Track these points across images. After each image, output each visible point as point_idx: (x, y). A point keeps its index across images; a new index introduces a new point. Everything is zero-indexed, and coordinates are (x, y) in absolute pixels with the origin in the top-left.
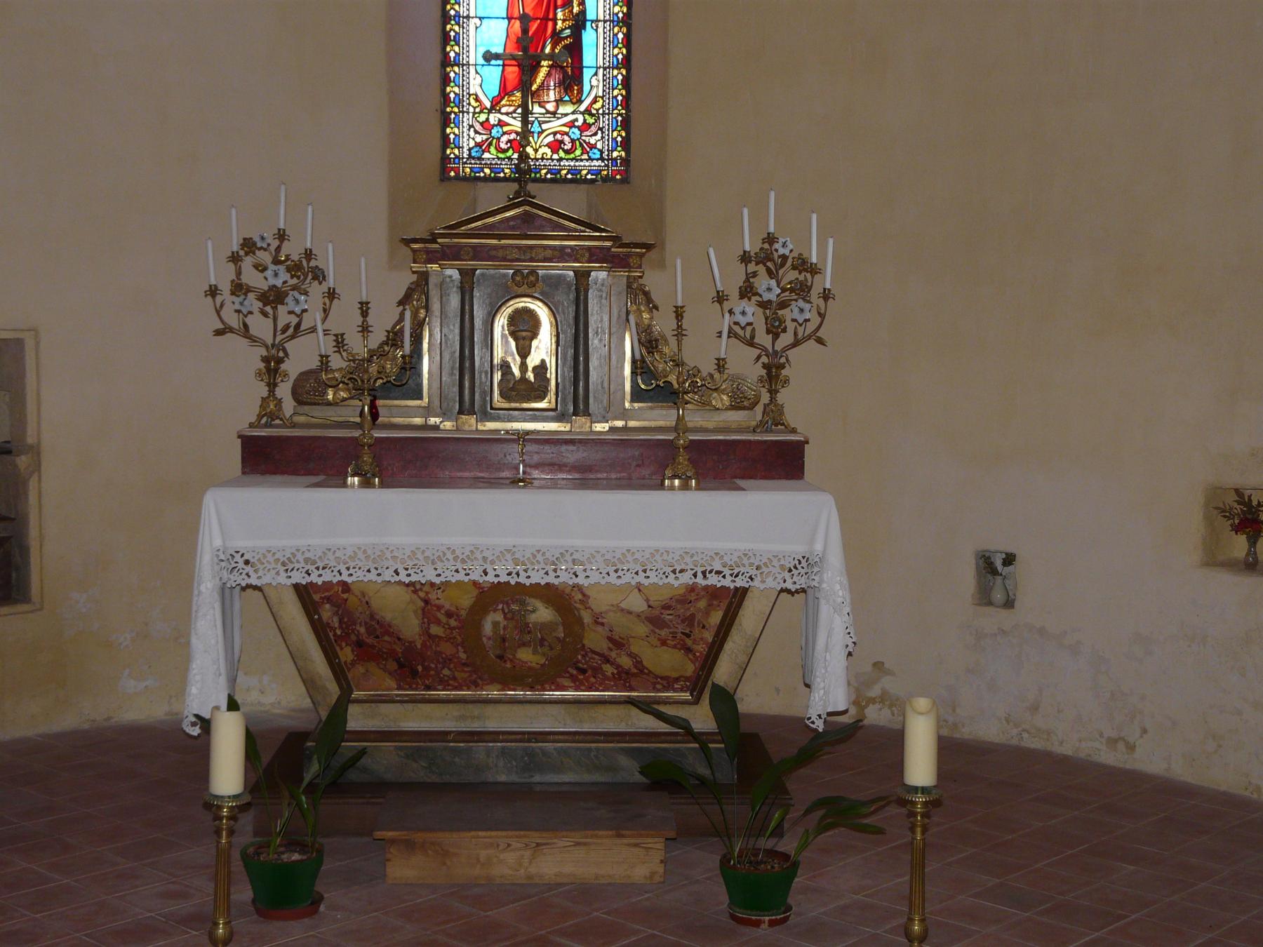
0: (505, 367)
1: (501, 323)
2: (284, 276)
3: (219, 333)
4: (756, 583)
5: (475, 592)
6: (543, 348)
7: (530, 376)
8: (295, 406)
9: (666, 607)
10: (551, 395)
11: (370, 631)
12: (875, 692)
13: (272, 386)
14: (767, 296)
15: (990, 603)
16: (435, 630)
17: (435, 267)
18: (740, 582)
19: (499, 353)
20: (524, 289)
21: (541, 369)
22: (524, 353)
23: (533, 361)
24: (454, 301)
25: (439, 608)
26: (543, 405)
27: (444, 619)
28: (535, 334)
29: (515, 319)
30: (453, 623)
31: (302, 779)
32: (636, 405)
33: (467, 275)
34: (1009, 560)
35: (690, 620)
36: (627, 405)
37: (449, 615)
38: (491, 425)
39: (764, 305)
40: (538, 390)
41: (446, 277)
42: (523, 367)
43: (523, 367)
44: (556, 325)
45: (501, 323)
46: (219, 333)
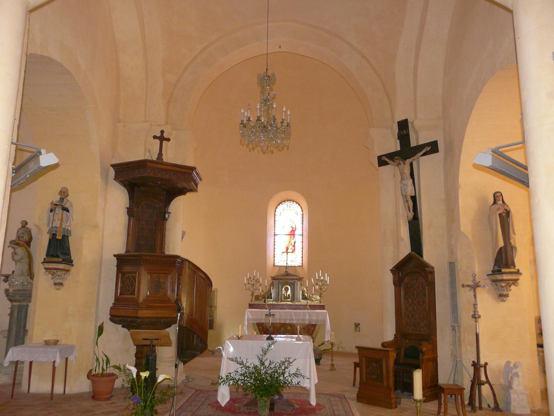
0: (284, 295)
1: (283, 289)
2: (255, 282)
3: (246, 290)
4: (317, 323)
5: (280, 325)
6: (289, 292)
7: (287, 296)
8: (132, 335)
9: (306, 327)
10: (290, 299)
11: (266, 330)
12: (340, 346)
13: (252, 297)
14: (319, 285)
15: (356, 331)
16: (275, 330)
17: (275, 281)
18: (315, 323)
19: (283, 293)
20: (287, 284)
21: (289, 295)
22: (287, 293)
23: (288, 294)
24: (277, 286)
25: (275, 327)
26: (289, 300)
27: (276, 328)
28: (288, 290)
29: (285, 288)
30: (277, 329)
31: (285, 288)
32: (302, 300)
33: (279, 282)
34: (359, 324)
35: (309, 329)
36: (301, 300)
37: (277, 328)
38: (282, 303)
39: (319, 286)
40: (289, 298)
41: (325, 342)
42: (286, 295)
43: (286, 295)
44: (291, 289)
45: (283, 289)
46: (246, 290)
